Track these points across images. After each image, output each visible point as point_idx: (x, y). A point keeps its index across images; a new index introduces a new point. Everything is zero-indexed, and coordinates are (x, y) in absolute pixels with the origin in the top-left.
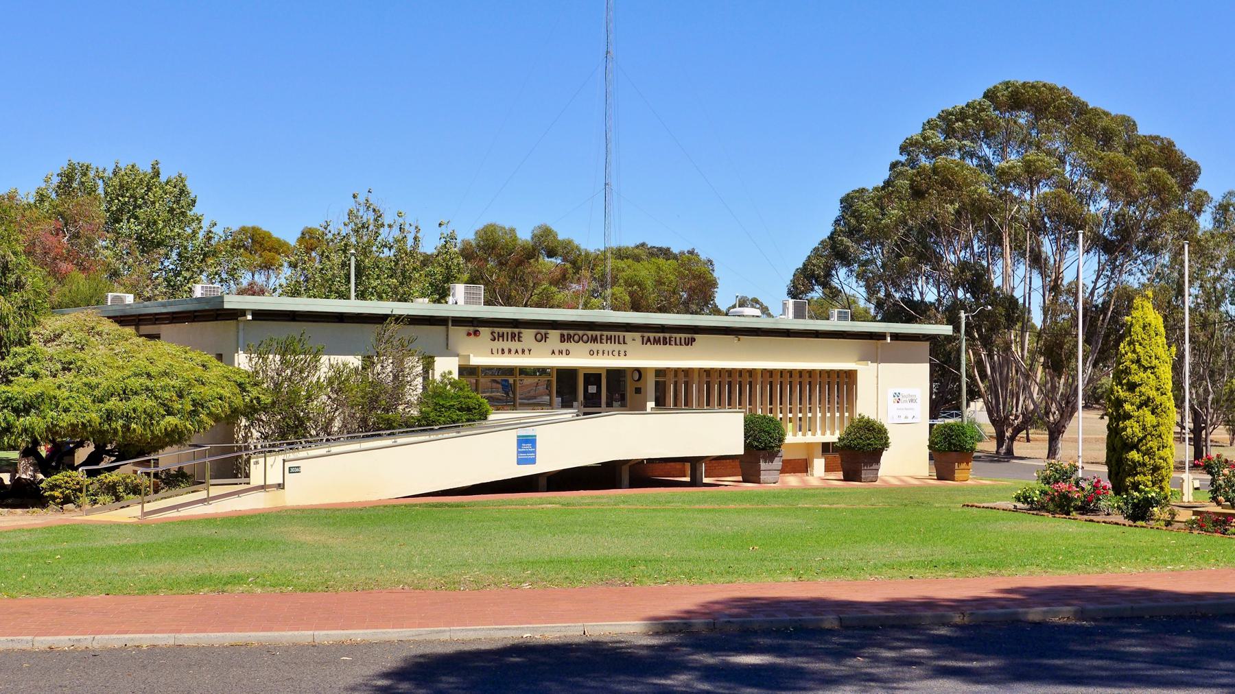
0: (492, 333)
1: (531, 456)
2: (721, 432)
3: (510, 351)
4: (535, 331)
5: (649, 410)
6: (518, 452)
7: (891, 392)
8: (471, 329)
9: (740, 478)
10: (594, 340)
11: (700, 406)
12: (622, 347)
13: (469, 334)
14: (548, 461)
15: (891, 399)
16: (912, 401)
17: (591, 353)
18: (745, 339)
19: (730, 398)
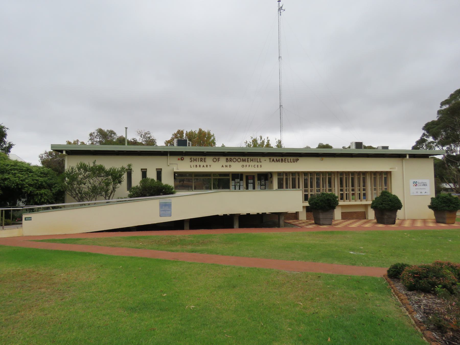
0: (191, 159)
1: (20, 222)
2: (291, 201)
3: (200, 166)
4: (190, 157)
5: (274, 189)
6: (160, 211)
7: (411, 182)
8: (180, 157)
9: (313, 222)
10: (244, 161)
11: (214, 188)
12: (259, 164)
13: (179, 159)
14: (175, 217)
15: (411, 184)
16: (424, 185)
17: (243, 166)
18: (325, 159)
19: (287, 184)
